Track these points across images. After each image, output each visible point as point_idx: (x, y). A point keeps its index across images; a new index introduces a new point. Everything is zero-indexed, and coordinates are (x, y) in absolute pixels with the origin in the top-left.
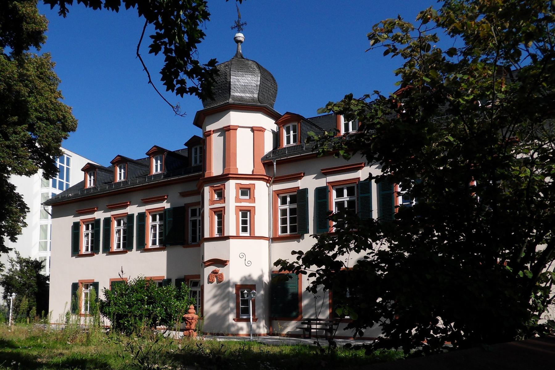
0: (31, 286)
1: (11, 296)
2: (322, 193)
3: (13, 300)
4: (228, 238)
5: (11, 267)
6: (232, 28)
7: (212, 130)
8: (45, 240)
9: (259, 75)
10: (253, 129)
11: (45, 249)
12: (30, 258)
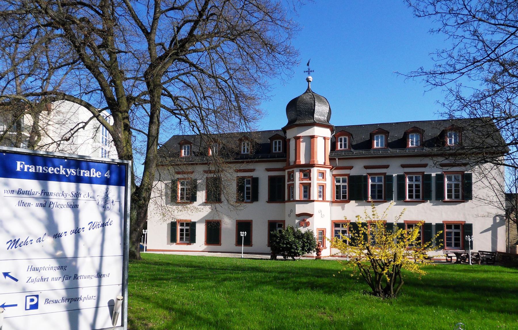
2: (401, 179)
4: (313, 201)
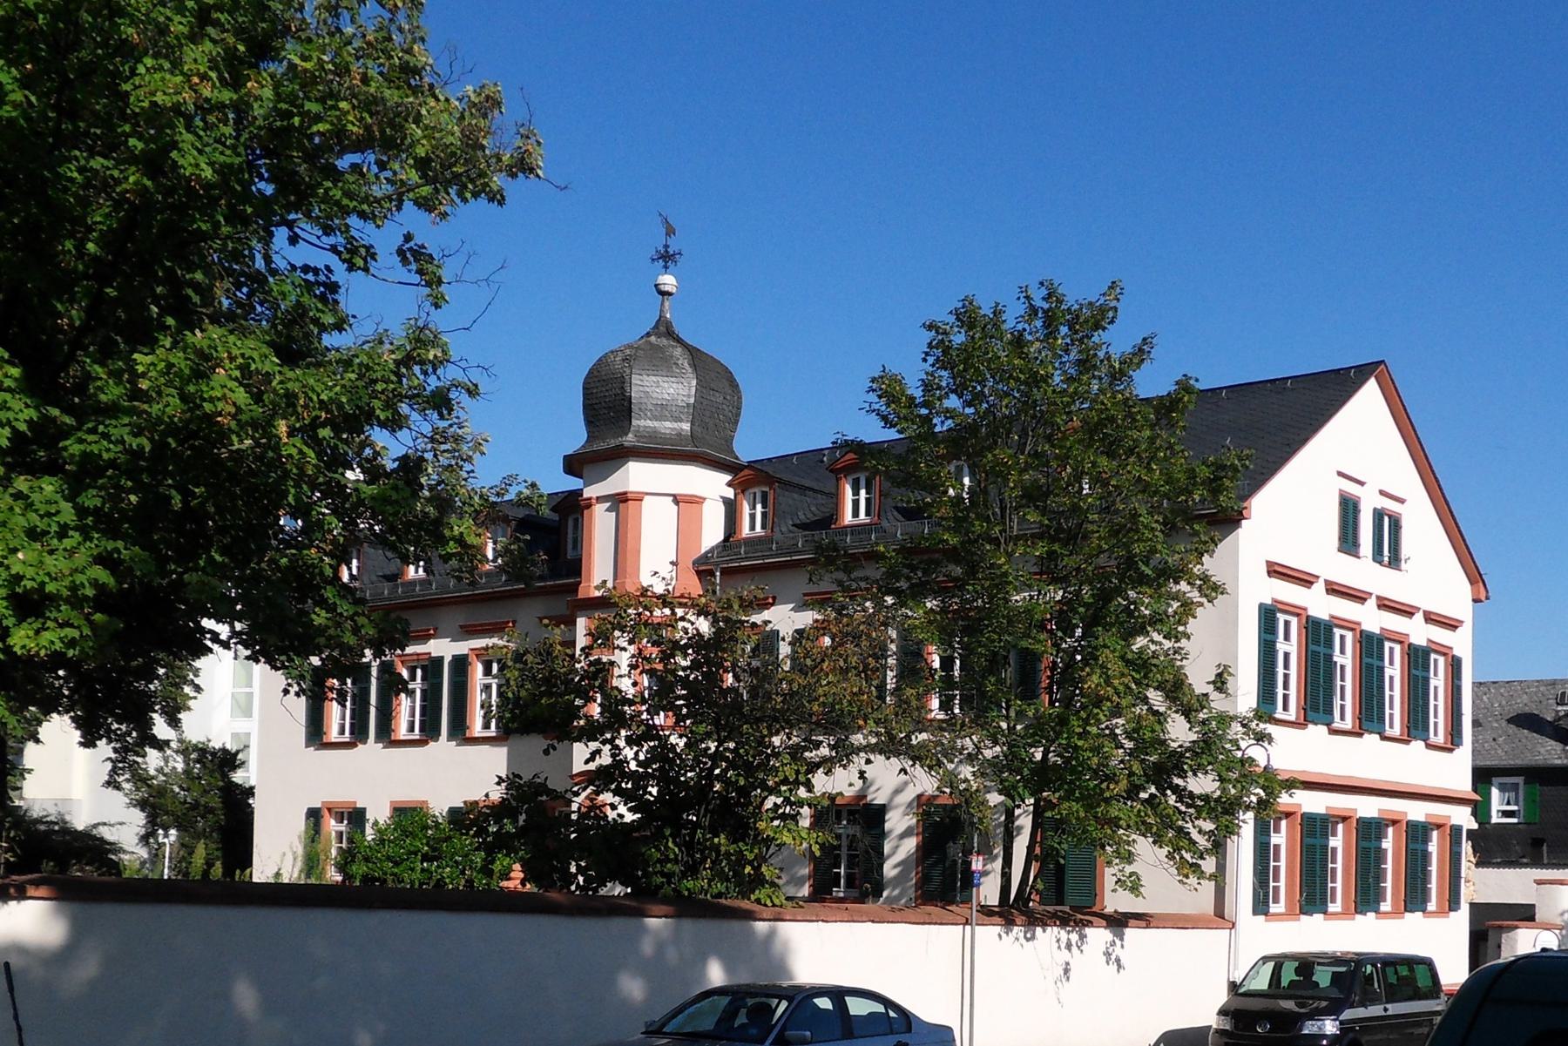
0: (211, 811)
1: (166, 836)
3: (171, 845)
5: (162, 764)
6: (653, 260)
7: (594, 496)
8: (248, 690)
9: (694, 382)
10: (677, 500)
11: (247, 713)
12: (209, 741)
